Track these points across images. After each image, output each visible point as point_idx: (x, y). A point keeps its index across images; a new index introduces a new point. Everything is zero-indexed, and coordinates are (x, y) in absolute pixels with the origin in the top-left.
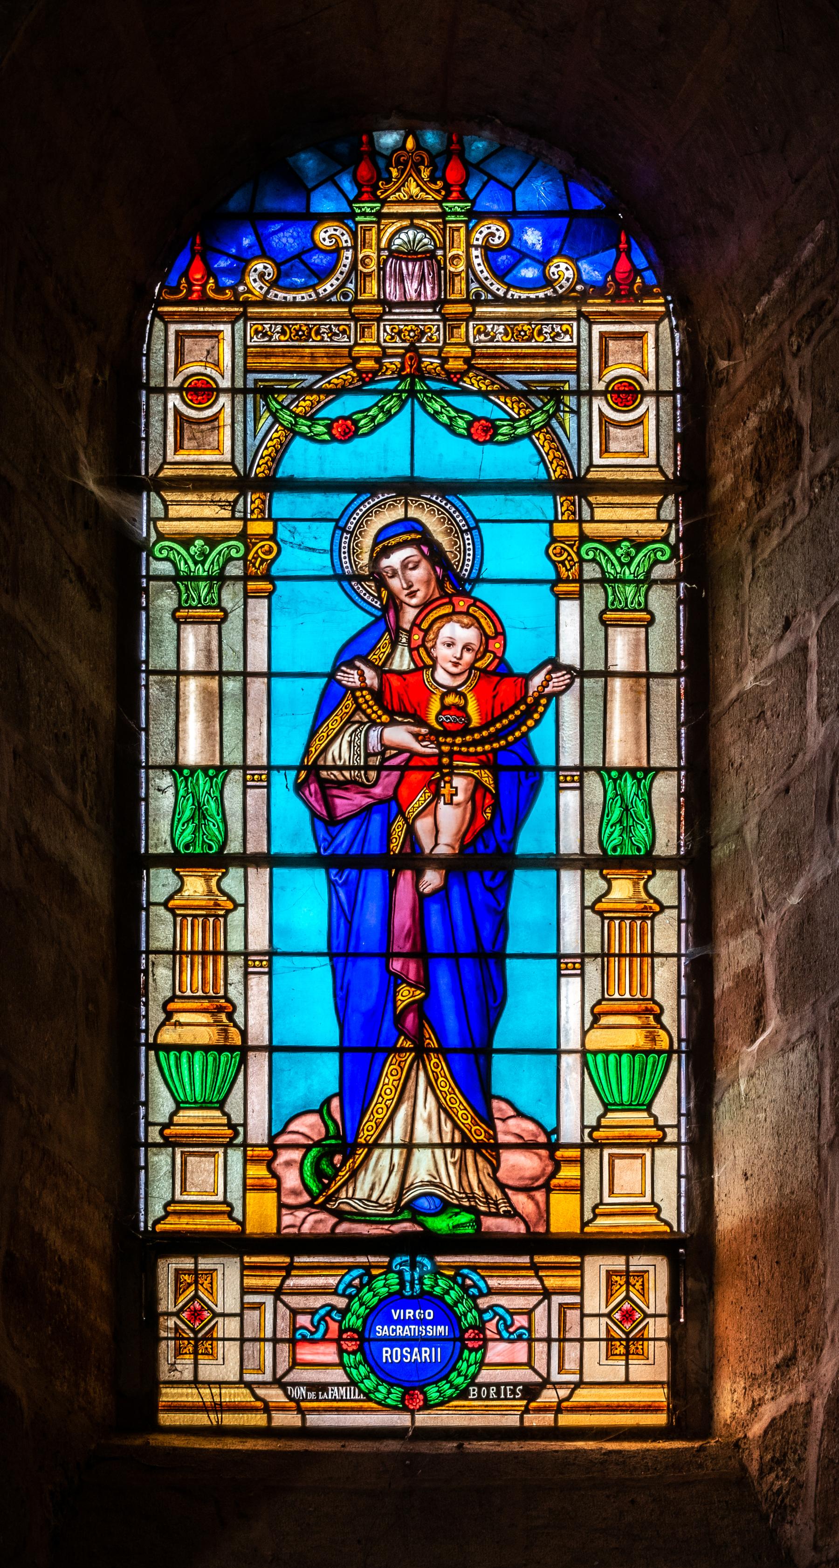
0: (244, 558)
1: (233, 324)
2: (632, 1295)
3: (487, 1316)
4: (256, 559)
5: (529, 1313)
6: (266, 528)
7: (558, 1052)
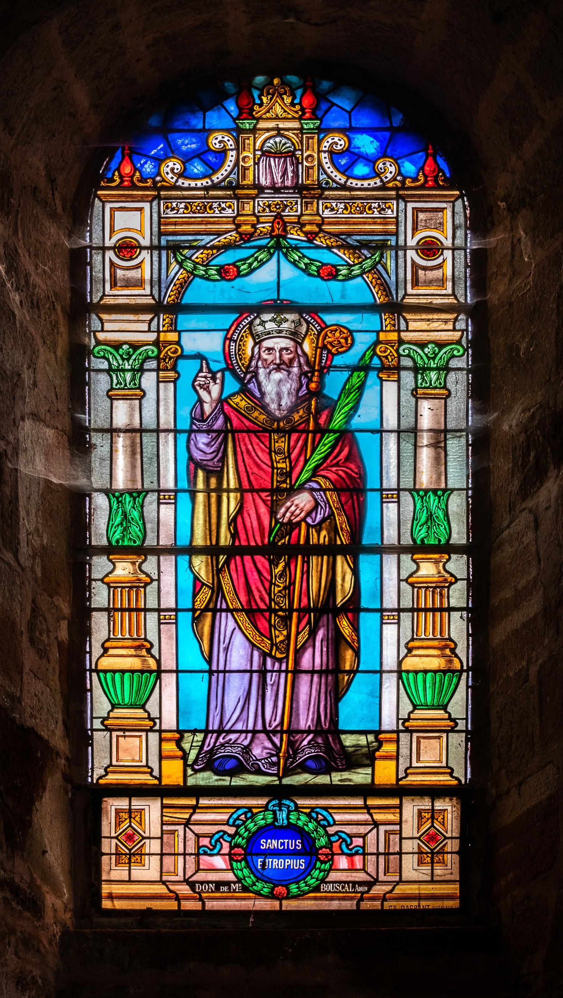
1: (151, 202)
2: (133, 824)
3: (334, 839)
4: (166, 357)
5: (364, 836)
7: (381, 672)
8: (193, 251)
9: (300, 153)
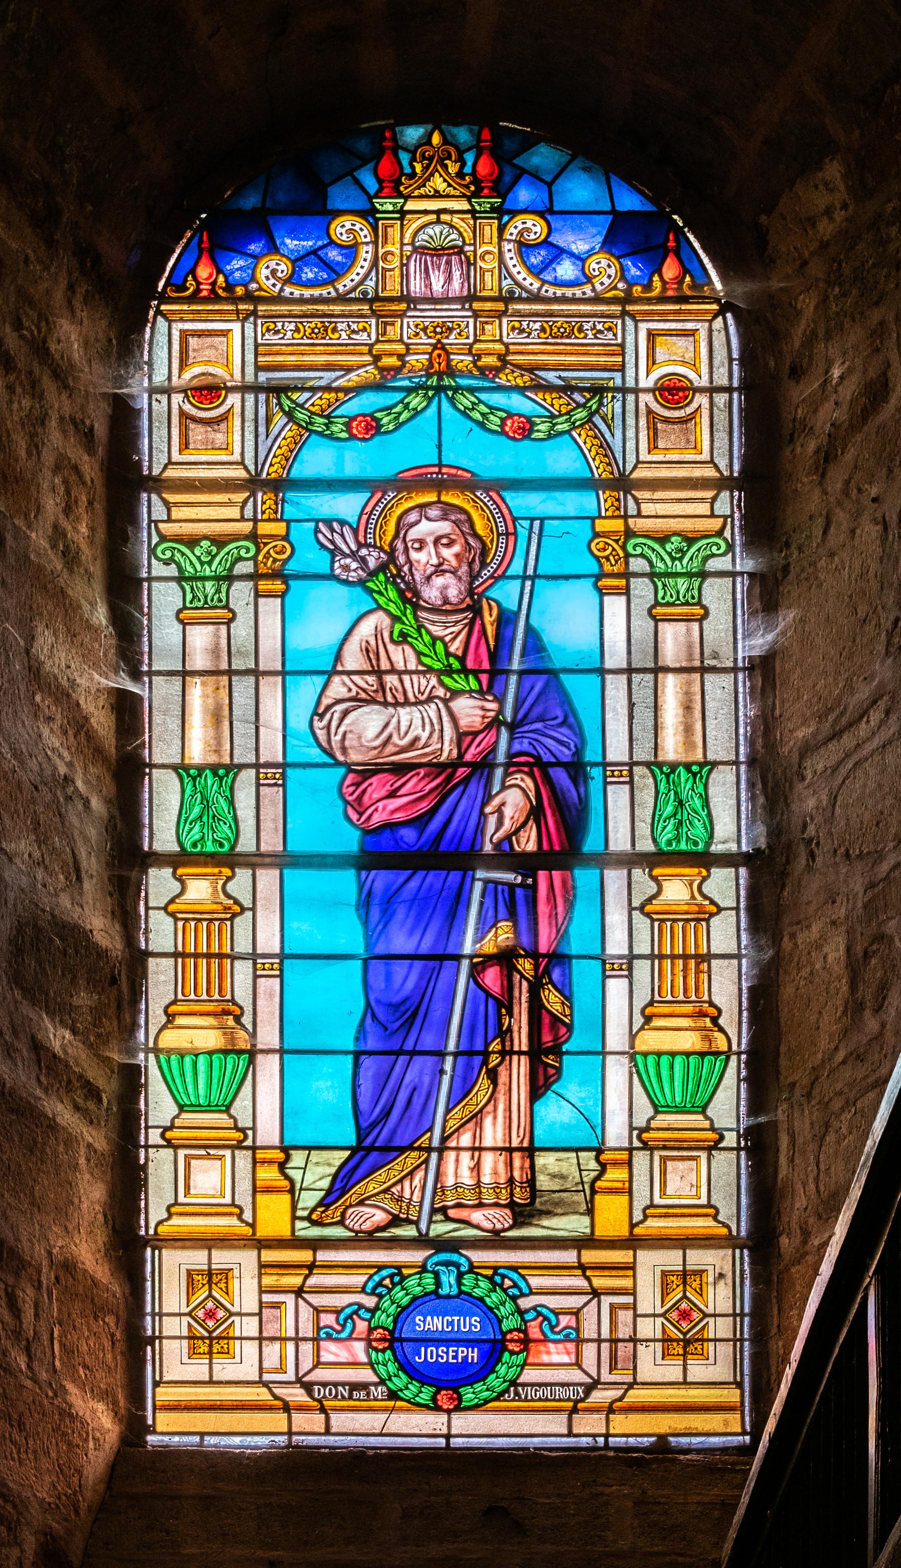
0: (254, 558)
6: (279, 528)
7: (604, 1053)
8: (307, 395)
9: (472, 248)
